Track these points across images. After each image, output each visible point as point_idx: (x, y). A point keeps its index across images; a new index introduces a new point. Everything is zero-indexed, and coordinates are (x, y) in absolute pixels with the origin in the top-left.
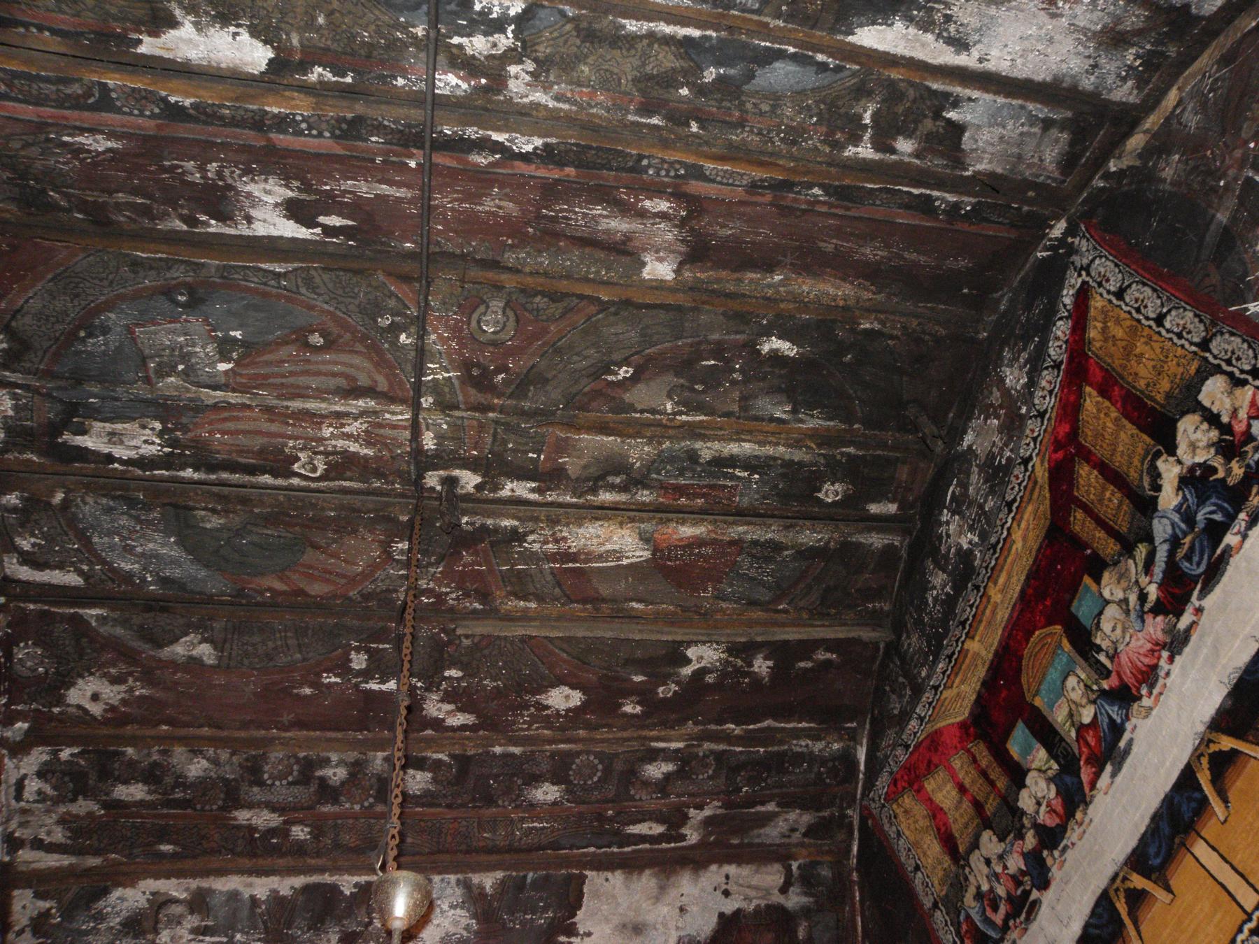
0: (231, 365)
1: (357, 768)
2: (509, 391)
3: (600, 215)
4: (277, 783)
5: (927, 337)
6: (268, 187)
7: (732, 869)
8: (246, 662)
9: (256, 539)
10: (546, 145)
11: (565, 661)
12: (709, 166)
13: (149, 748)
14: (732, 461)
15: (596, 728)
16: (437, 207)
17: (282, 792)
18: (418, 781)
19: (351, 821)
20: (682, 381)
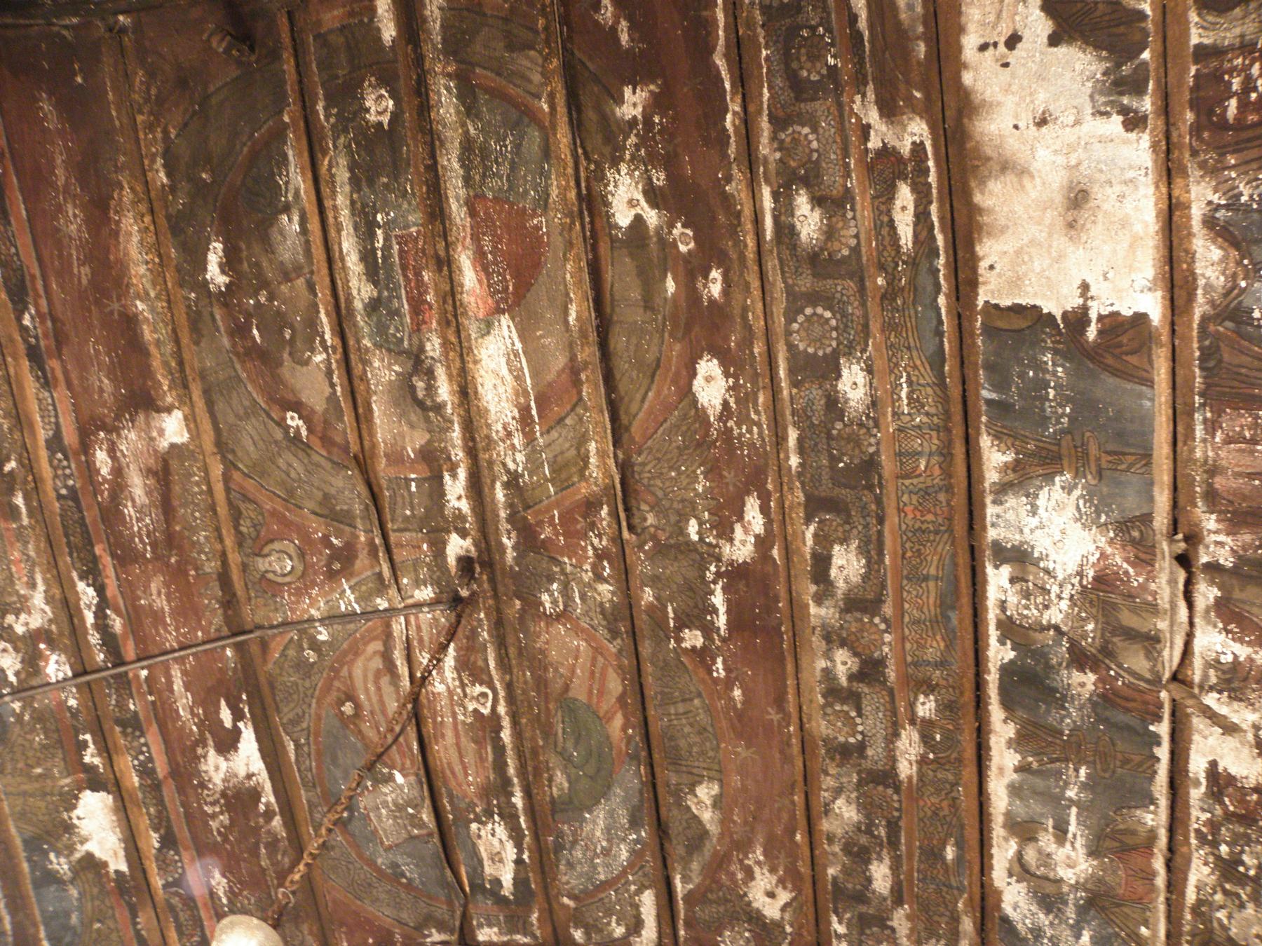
0: (395, 772)
1: (832, 638)
2: (347, 529)
3: (134, 506)
4: (860, 728)
5: (153, 91)
6: (212, 768)
7: (970, 42)
8: (711, 754)
9: (570, 745)
10: (81, 578)
11: (659, 393)
12: (43, 434)
13: (827, 853)
14: (367, 256)
15: (748, 327)
16: (179, 642)
17: (872, 723)
18: (847, 565)
19: (908, 646)
20: (286, 356)
